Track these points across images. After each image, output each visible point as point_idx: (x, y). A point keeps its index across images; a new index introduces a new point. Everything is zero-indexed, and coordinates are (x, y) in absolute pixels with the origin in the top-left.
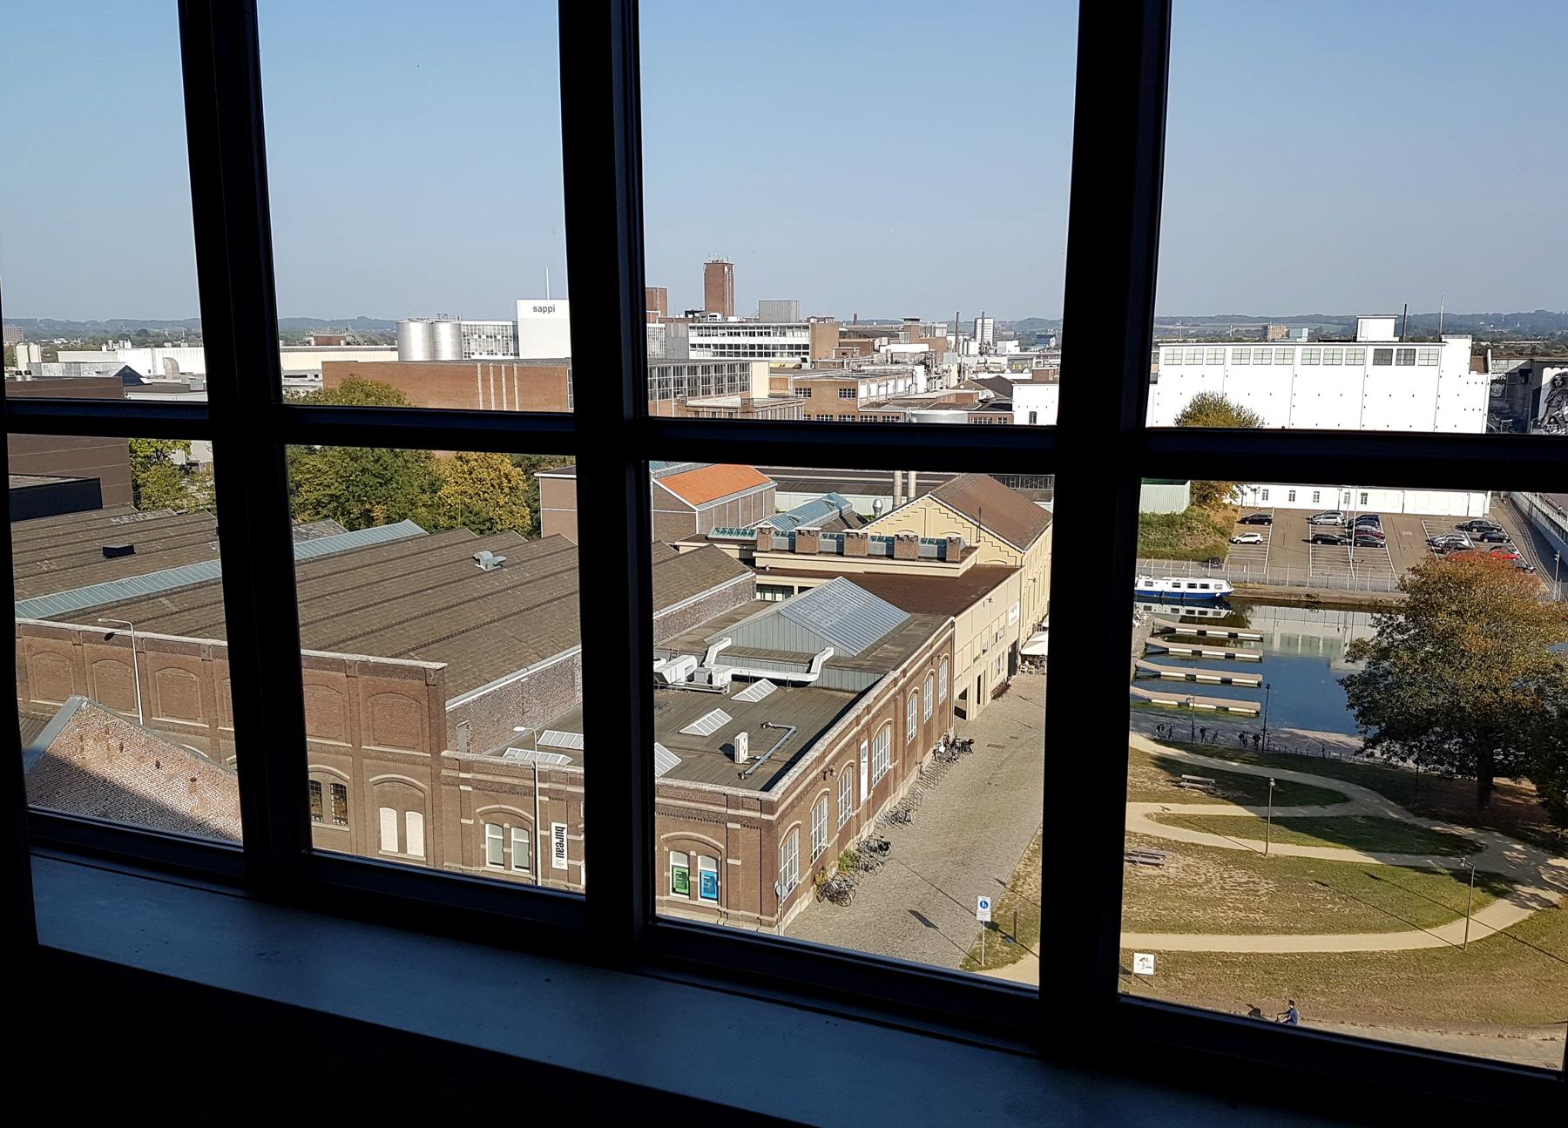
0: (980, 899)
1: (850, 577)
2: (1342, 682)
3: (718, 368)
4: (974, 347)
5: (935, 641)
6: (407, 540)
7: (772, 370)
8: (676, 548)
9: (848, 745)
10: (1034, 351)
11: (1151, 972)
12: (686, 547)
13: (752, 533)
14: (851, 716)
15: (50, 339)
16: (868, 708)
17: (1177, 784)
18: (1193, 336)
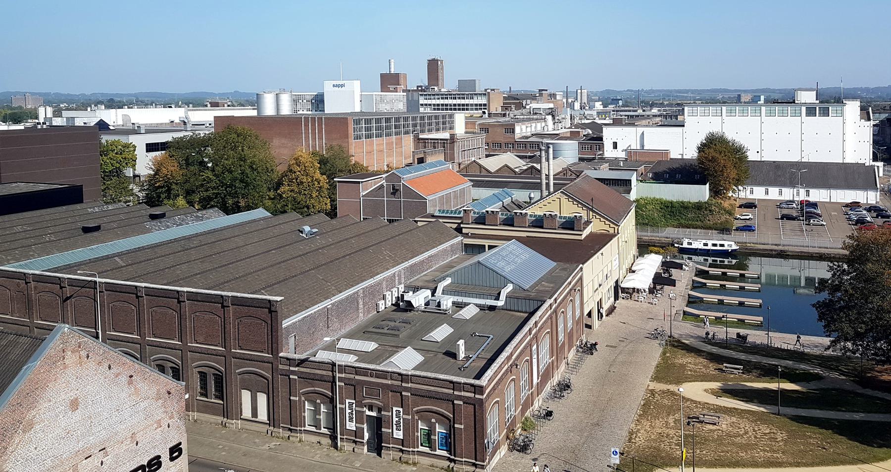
1: (519, 239)
2: (814, 305)
3: (436, 117)
5: (572, 280)
6: (261, 219)
8: (416, 222)
9: (525, 348)
10: (611, 107)
14: (526, 329)
15: (58, 104)
18: (698, 100)
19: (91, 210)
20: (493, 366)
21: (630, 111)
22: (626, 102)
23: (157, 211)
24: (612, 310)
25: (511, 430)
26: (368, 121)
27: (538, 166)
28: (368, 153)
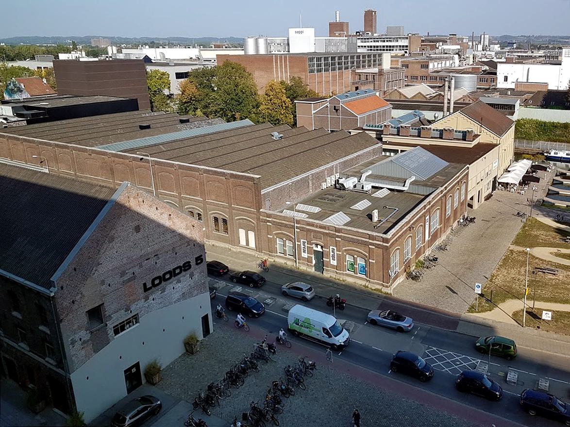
0: (477, 284)
1: (423, 146)
3: (369, 56)
4: (480, 47)
5: (460, 175)
7: (392, 57)
8: (350, 132)
10: (507, 49)
11: (550, 319)
12: (353, 132)
13: (381, 127)
14: (422, 205)
15: (120, 44)
16: (429, 203)
17: (564, 240)
19: (144, 115)
20: (396, 227)
21: (521, 52)
22: (519, 45)
23: (184, 118)
24: (489, 197)
25: (408, 266)
26: (319, 59)
27: (442, 93)
28: (320, 83)
